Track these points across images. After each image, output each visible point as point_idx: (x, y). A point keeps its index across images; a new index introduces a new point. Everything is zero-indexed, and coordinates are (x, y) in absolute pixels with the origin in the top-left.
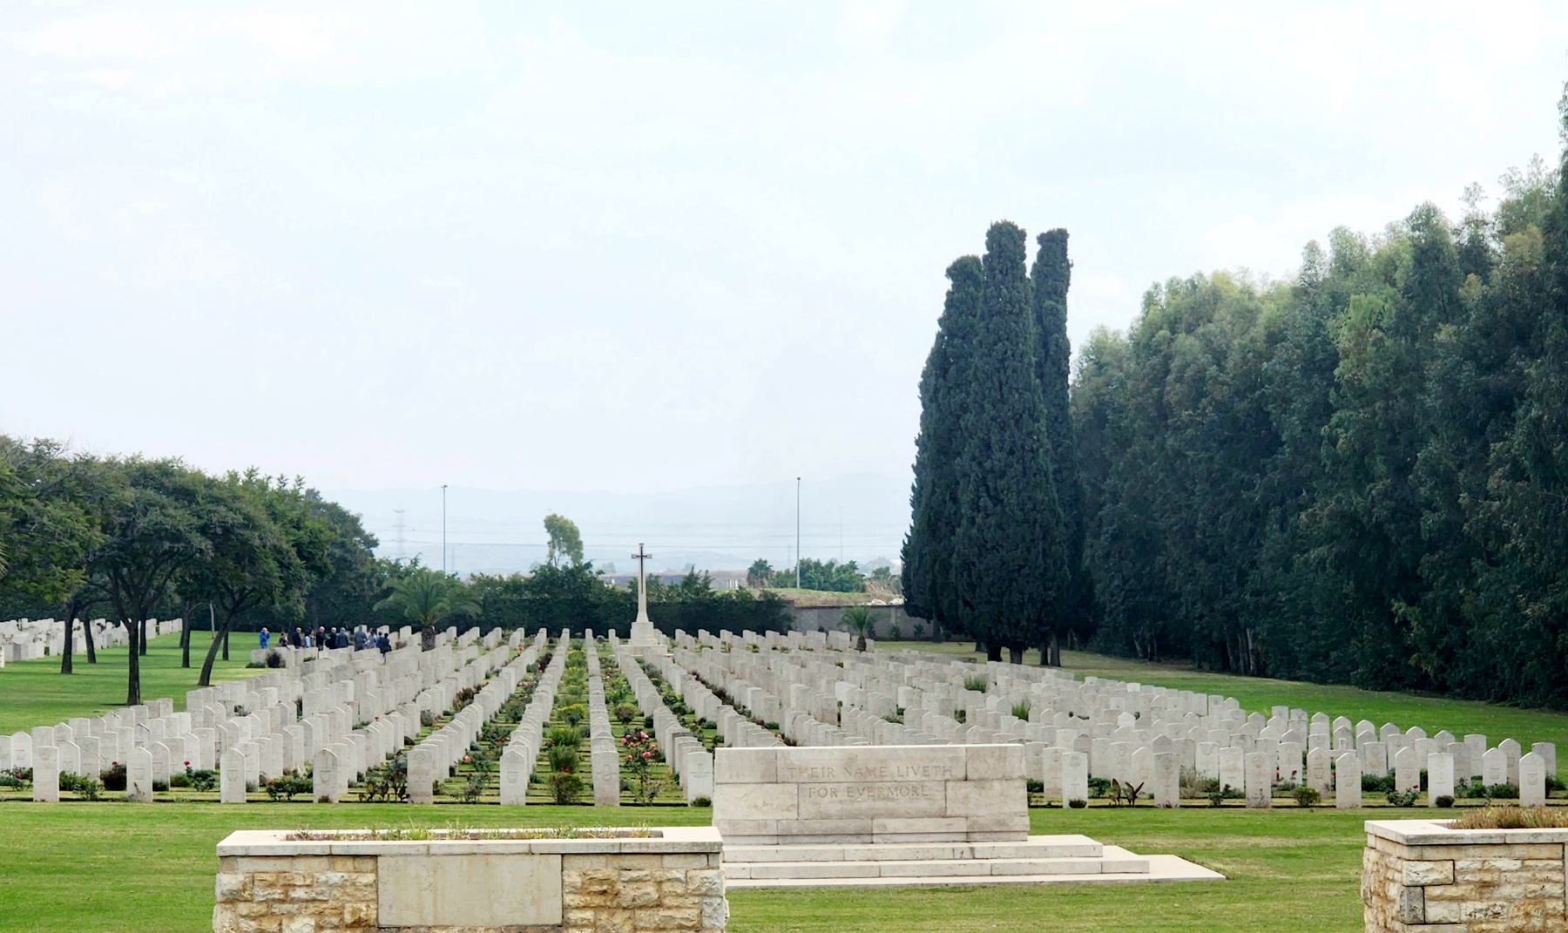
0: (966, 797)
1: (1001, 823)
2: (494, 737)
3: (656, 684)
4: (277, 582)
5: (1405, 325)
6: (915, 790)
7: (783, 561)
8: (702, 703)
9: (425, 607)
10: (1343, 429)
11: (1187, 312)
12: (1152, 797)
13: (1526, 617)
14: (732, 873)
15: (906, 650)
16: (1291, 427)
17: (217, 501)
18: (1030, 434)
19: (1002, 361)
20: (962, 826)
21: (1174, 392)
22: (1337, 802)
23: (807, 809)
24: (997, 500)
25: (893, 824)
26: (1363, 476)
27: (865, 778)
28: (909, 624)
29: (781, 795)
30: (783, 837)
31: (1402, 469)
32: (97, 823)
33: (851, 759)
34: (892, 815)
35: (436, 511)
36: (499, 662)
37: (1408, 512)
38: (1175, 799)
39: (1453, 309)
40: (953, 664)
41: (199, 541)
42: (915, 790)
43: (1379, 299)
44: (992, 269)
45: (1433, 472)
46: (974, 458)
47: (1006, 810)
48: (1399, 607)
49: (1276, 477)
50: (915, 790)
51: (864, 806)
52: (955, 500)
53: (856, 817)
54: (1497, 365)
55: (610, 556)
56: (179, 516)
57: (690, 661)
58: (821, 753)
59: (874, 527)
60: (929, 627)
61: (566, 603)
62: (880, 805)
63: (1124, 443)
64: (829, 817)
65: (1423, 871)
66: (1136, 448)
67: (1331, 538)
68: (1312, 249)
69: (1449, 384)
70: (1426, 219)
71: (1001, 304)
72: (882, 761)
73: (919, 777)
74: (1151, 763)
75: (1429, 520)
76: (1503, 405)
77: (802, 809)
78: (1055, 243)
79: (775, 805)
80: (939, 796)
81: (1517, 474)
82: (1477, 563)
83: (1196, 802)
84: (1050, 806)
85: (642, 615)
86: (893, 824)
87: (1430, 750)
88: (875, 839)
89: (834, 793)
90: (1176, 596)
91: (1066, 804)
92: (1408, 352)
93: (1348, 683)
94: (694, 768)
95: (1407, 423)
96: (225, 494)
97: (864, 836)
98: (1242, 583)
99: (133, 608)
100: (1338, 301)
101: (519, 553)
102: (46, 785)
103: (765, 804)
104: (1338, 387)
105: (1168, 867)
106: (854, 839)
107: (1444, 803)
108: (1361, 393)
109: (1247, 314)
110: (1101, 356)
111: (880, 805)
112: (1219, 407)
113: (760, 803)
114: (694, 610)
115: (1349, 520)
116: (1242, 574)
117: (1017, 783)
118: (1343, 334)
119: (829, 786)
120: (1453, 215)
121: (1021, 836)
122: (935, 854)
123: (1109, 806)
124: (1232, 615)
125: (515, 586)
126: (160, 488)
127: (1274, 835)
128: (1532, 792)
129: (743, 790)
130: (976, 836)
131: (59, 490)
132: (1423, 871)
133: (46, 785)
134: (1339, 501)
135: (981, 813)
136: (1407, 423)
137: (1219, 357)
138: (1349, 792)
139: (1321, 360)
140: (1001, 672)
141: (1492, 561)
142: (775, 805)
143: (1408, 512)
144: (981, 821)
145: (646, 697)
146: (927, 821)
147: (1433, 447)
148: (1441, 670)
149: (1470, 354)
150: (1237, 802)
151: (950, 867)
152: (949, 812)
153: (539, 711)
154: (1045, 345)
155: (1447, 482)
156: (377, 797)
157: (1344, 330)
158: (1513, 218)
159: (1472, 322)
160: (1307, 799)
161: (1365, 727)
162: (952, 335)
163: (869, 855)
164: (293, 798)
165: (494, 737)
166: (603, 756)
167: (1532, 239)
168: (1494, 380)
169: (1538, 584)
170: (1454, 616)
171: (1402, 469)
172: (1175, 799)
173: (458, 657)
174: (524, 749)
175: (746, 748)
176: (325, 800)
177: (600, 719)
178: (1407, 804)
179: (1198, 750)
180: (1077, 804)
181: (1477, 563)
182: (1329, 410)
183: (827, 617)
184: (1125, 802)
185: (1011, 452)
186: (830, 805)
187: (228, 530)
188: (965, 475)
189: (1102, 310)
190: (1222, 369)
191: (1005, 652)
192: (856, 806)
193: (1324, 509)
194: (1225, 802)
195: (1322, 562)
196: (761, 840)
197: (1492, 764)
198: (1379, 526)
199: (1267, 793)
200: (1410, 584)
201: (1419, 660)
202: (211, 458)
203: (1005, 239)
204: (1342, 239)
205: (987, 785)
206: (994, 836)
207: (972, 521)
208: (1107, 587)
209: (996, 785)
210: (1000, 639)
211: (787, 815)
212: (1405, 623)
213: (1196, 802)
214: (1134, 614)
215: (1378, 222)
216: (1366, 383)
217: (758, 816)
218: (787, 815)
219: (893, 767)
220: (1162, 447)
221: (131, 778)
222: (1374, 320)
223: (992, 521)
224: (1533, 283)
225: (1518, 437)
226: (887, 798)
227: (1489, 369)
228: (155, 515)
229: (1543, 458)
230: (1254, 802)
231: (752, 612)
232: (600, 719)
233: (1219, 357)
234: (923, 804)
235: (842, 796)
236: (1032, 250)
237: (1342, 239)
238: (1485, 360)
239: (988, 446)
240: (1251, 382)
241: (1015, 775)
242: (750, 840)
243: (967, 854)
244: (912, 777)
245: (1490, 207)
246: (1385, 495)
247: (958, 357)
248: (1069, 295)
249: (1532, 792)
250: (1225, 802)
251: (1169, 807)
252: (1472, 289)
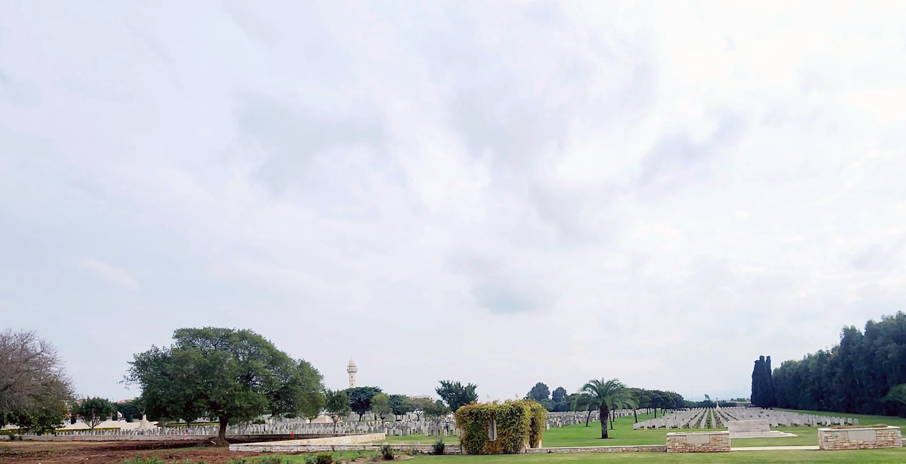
2: (700, 421)
5: (818, 364)
7: (735, 398)
8: (726, 416)
11: (787, 365)
14: (731, 436)
16: (803, 379)
21: (786, 375)
27: (748, 424)
31: (819, 383)
32: (652, 431)
35: (690, 394)
36: (700, 411)
39: (826, 362)
40: (759, 410)
43: (815, 361)
55: (713, 399)
56: (660, 396)
57: (723, 411)
58: (742, 421)
59: (746, 392)
61: (708, 404)
65: (827, 435)
70: (821, 351)
71: (762, 366)
76: (834, 374)
78: (768, 358)
79: (736, 428)
87: (827, 419)
94: (725, 424)
99: (655, 407)
100: (809, 362)
101: (702, 399)
102: (646, 428)
105: (790, 435)
110: (776, 370)
114: (724, 404)
118: (810, 366)
120: (824, 350)
128: (842, 423)
131: (268, 348)
132: (827, 435)
133: (646, 428)
138: (815, 425)
139: (807, 369)
140: (765, 411)
142: (736, 428)
145: (719, 415)
153: (705, 417)
158: (833, 350)
165: (700, 421)
166: (714, 422)
167: (836, 353)
169: (841, 397)
171: (819, 383)
173: (695, 411)
174: (704, 422)
175: (732, 421)
177: (713, 418)
178: (824, 426)
183: (741, 405)
189: (775, 365)
193: (808, 389)
197: (836, 420)
202: (663, 389)
203: (762, 358)
204: (809, 355)
210: (765, 406)
215: (814, 352)
222: (814, 364)
224: (838, 358)
225: (836, 378)
231: (732, 405)
232: (713, 418)
237: (809, 355)
240: (797, 373)
245: (830, 349)
249: (842, 423)
252: (828, 359)
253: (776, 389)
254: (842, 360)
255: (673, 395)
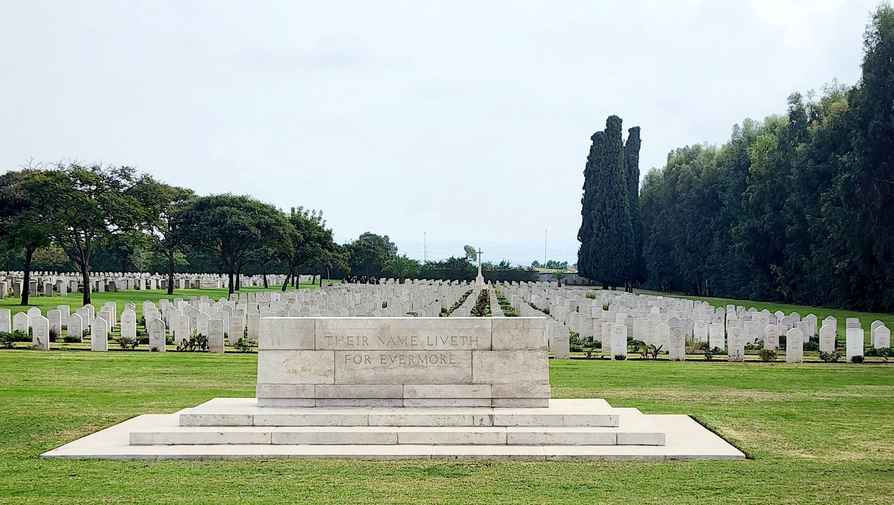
0: (492, 365)
1: (522, 390)
3: (466, 297)
4: (292, 249)
5: (783, 145)
6: (444, 358)
9: (401, 270)
10: (752, 193)
11: (685, 162)
12: (667, 353)
13: (836, 269)
15: (575, 288)
16: (727, 197)
17: (265, 213)
18: (621, 201)
19: (611, 172)
20: (487, 392)
22: (787, 358)
23: (343, 375)
24: (607, 227)
25: (422, 390)
26: (760, 212)
28: (580, 279)
29: (320, 361)
30: (321, 400)
31: (777, 209)
33: (384, 329)
34: (423, 381)
37: (780, 228)
38: (683, 356)
39: (805, 137)
41: (254, 230)
42: (443, 358)
44: (608, 135)
45: (793, 207)
46: (599, 210)
47: (528, 378)
48: (773, 267)
49: (720, 218)
50: (444, 358)
51: (396, 372)
52: (592, 228)
53: (388, 382)
54: (824, 160)
56: (246, 219)
60: (587, 281)
62: (410, 371)
63: (659, 211)
64: (363, 382)
66: (664, 211)
67: (744, 238)
68: (736, 126)
69: (802, 169)
71: (611, 152)
72: (413, 331)
73: (447, 346)
74: (667, 331)
75: (789, 229)
76: (826, 178)
77: (339, 375)
78: (635, 132)
80: (466, 364)
81: (837, 203)
82: (812, 246)
83: (695, 357)
84: (603, 358)
85: (480, 274)
86: (422, 390)
87: (793, 326)
88: (406, 403)
89: (368, 359)
90: (678, 267)
91: (613, 357)
92: (783, 157)
93: (748, 299)
95: (781, 188)
96: (268, 211)
97: (395, 400)
98: (704, 262)
103: (304, 370)
104: (750, 175)
106: (386, 403)
107: (857, 360)
108: (761, 178)
109: (710, 155)
110: (651, 178)
111: (410, 371)
112: (698, 192)
113: (299, 369)
115: (752, 231)
116: (705, 257)
117: (539, 354)
118: (753, 154)
119: (363, 354)
121: (543, 403)
122: (456, 421)
123: (640, 359)
124: (700, 274)
125: (441, 264)
126: (239, 207)
127: (761, 389)
129: (284, 356)
130: (500, 402)
134: (749, 223)
135: (504, 380)
136: (781, 188)
137: (698, 173)
141: (818, 244)
142: (312, 371)
143: (780, 228)
144: (506, 388)
146: (454, 387)
147: (793, 197)
148: (790, 293)
149: (811, 155)
150: (722, 357)
151: (467, 435)
152: (474, 381)
154: (630, 172)
155: (798, 212)
156: (188, 348)
157: (754, 152)
159: (813, 142)
160: (768, 357)
161: (780, 314)
162: (592, 164)
163: (392, 421)
164: (136, 348)
168: (822, 167)
169: (842, 253)
170: (798, 270)
172: (683, 356)
176: (155, 350)
179: (696, 324)
180: (619, 358)
181: (812, 246)
182: (746, 185)
184: (650, 356)
185: (614, 208)
186: (364, 371)
187: (268, 226)
188: (595, 217)
189: (652, 161)
190: (699, 177)
191: (610, 288)
192: (389, 372)
193: (743, 226)
194: (715, 357)
195: (741, 248)
196: (301, 403)
198: (767, 232)
199: (742, 351)
200: (779, 257)
201: (781, 289)
203: (614, 123)
205: (511, 354)
206: (517, 402)
207: (598, 235)
208: (652, 265)
209: (520, 355)
210: (609, 282)
211: (324, 379)
212: (776, 274)
213: (695, 357)
214: (661, 275)
216: (763, 173)
217: (297, 380)
218: (324, 379)
219: (423, 337)
220: (674, 210)
221: (35, 337)
223: (605, 235)
226: (417, 366)
227: (819, 162)
228: (235, 218)
229: (850, 196)
230: (733, 358)
231: (527, 276)
233: (698, 173)
234: (451, 372)
235: (376, 363)
236: (625, 135)
238: (818, 159)
239: (605, 206)
241: (537, 346)
242: (290, 403)
243: (487, 421)
244: (440, 346)
246: (770, 220)
247: (594, 172)
248: (640, 153)
250: (715, 357)
251: (678, 360)
253: (650, 230)
254: (863, 126)
255: (242, 204)
